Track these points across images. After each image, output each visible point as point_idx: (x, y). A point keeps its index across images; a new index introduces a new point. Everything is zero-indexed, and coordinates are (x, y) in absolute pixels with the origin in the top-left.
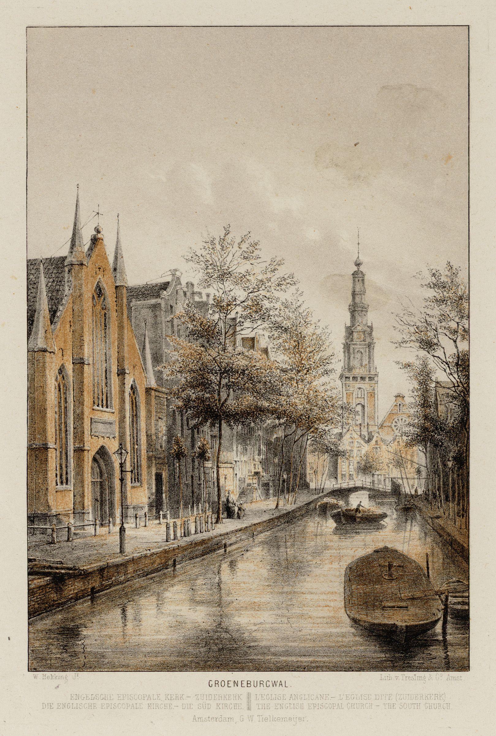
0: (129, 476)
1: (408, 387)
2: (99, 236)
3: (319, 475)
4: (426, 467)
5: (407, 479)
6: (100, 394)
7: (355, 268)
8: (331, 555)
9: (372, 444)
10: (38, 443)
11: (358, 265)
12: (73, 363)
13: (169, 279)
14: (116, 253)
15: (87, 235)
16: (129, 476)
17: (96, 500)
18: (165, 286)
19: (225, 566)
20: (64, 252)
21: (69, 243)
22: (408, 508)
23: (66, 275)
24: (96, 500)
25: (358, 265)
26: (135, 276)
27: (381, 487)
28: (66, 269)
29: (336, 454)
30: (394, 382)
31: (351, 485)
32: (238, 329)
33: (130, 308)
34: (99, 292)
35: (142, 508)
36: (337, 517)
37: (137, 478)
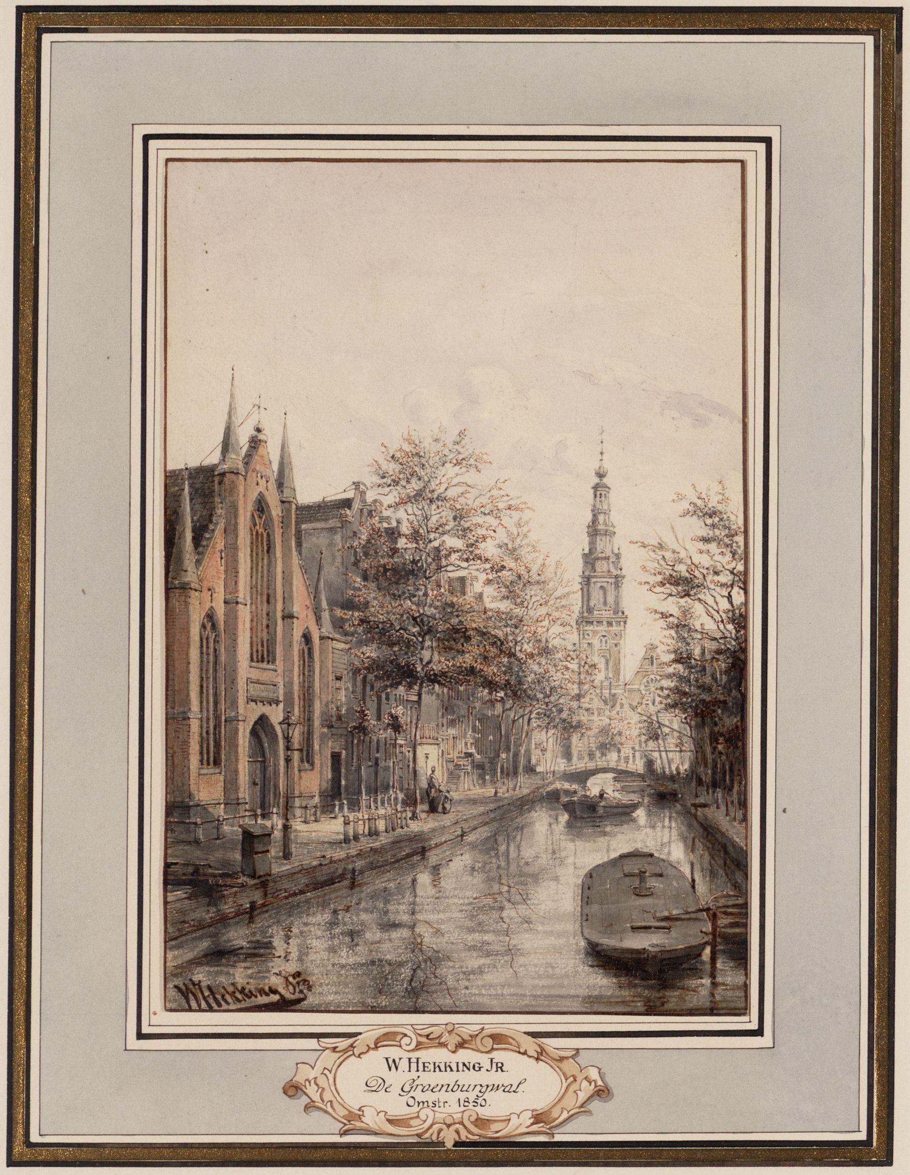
0: (296, 756)
1: (664, 641)
2: (261, 437)
3: (547, 755)
4: (691, 736)
5: (666, 751)
6: (260, 648)
7: (597, 480)
8: (562, 860)
9: (619, 693)
10: (178, 709)
11: (601, 476)
12: (225, 602)
13: (350, 495)
14: (282, 457)
15: (243, 437)
16: (296, 756)
17: (255, 784)
18: (347, 503)
19: (424, 878)
20: (214, 458)
21: (220, 449)
22: (664, 793)
23: (216, 487)
24: (255, 784)
25: (601, 476)
26: (308, 492)
27: (631, 767)
28: (217, 479)
29: (569, 727)
30: (645, 634)
31: (591, 765)
32: (444, 563)
33: (299, 533)
34: (261, 506)
35: (313, 797)
36: (569, 807)
37: (308, 757)
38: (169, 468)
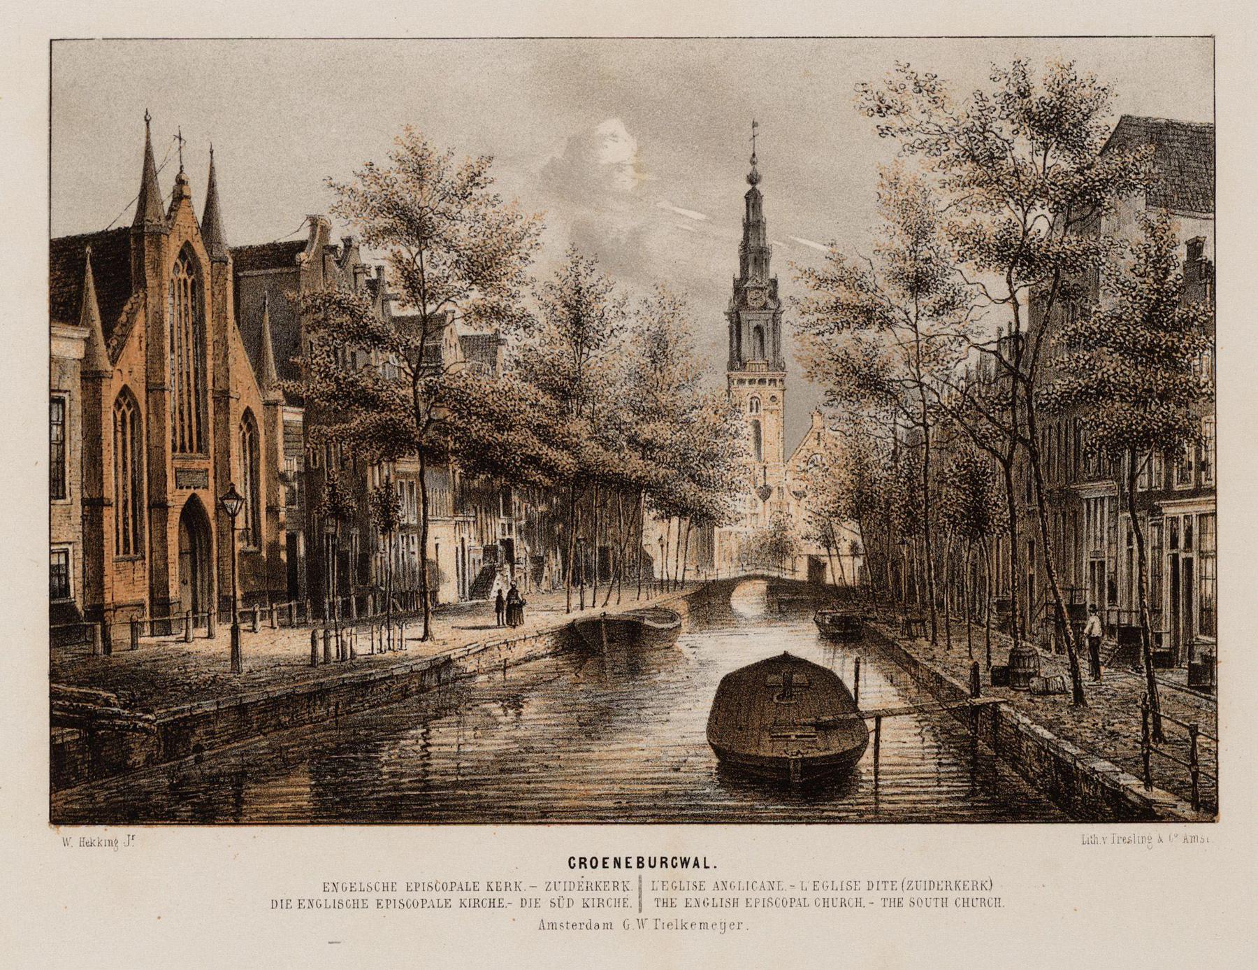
13: (304, 235)
18: (301, 246)
38: (55, 236)
